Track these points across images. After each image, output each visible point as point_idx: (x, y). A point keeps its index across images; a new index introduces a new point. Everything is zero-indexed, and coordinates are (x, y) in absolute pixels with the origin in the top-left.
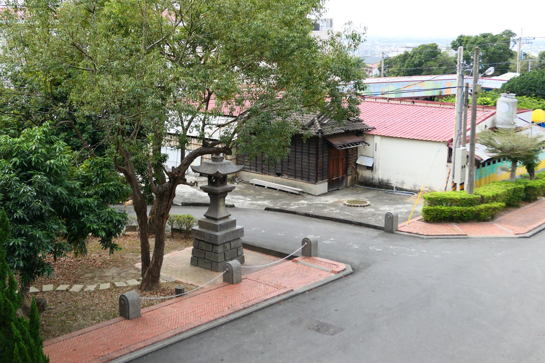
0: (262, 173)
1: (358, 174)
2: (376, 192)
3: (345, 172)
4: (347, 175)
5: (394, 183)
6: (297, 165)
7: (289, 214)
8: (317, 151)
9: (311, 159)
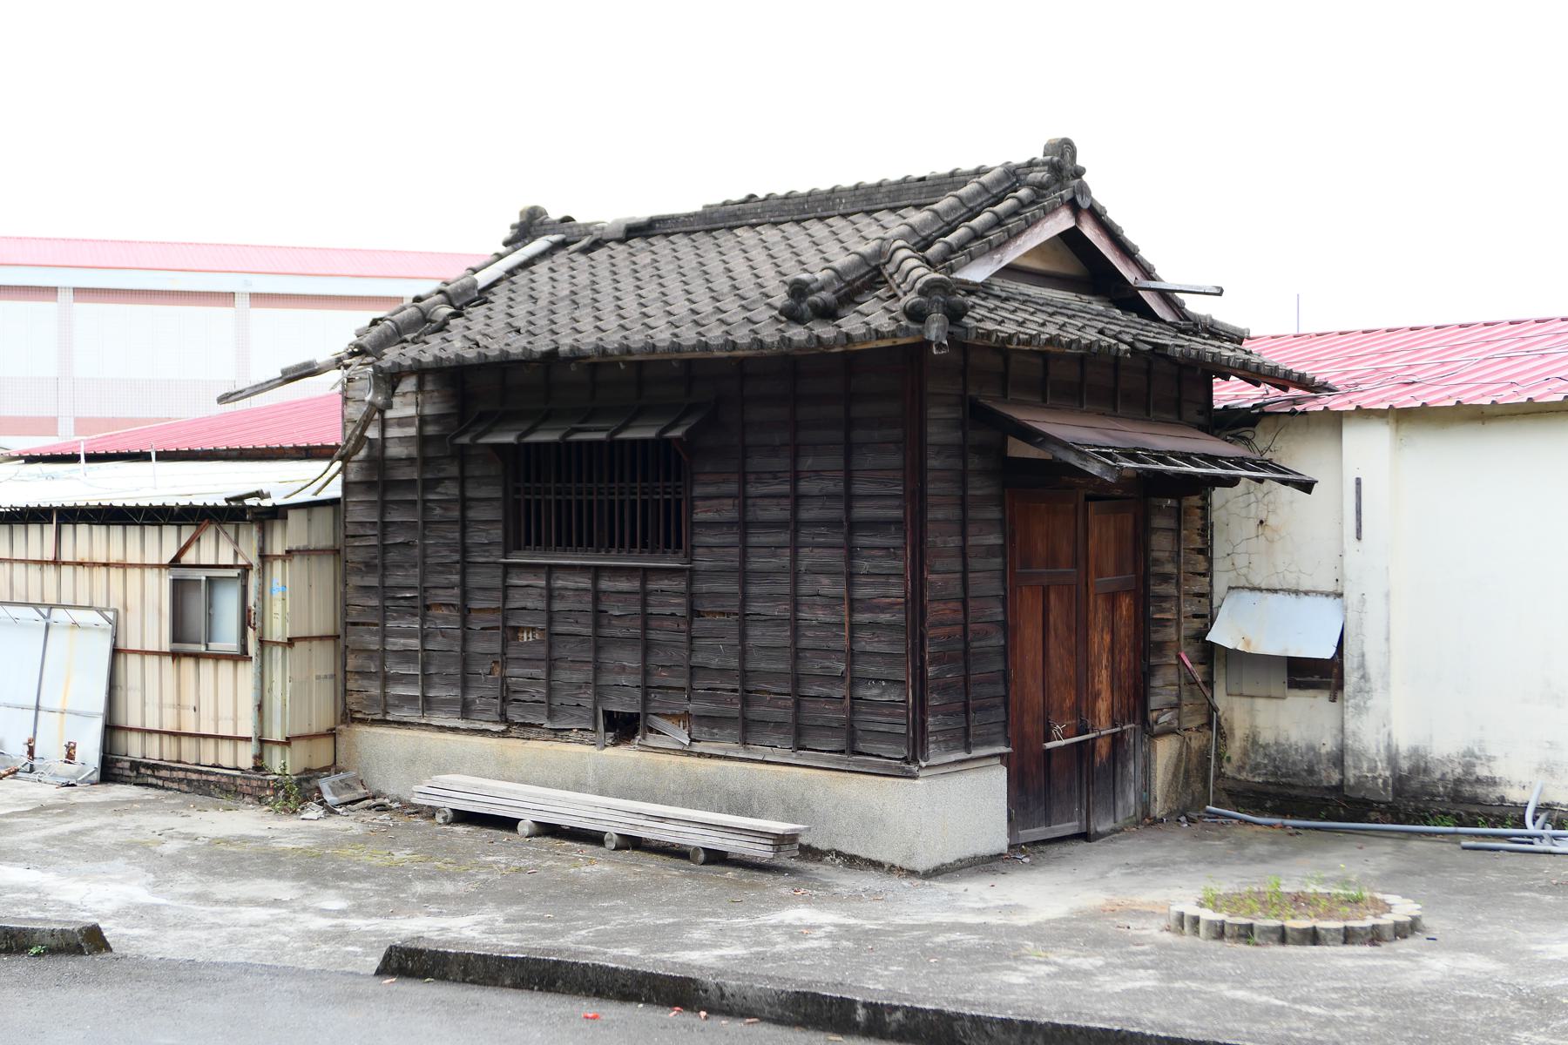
0: (510, 727)
1: (1222, 735)
2: (1387, 846)
3: (1135, 701)
4: (1150, 732)
5: (1520, 777)
6: (757, 635)
7: (613, 1011)
8: (917, 499)
9: (864, 565)
